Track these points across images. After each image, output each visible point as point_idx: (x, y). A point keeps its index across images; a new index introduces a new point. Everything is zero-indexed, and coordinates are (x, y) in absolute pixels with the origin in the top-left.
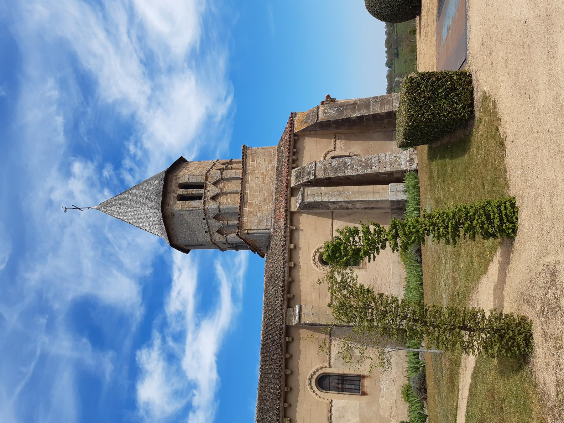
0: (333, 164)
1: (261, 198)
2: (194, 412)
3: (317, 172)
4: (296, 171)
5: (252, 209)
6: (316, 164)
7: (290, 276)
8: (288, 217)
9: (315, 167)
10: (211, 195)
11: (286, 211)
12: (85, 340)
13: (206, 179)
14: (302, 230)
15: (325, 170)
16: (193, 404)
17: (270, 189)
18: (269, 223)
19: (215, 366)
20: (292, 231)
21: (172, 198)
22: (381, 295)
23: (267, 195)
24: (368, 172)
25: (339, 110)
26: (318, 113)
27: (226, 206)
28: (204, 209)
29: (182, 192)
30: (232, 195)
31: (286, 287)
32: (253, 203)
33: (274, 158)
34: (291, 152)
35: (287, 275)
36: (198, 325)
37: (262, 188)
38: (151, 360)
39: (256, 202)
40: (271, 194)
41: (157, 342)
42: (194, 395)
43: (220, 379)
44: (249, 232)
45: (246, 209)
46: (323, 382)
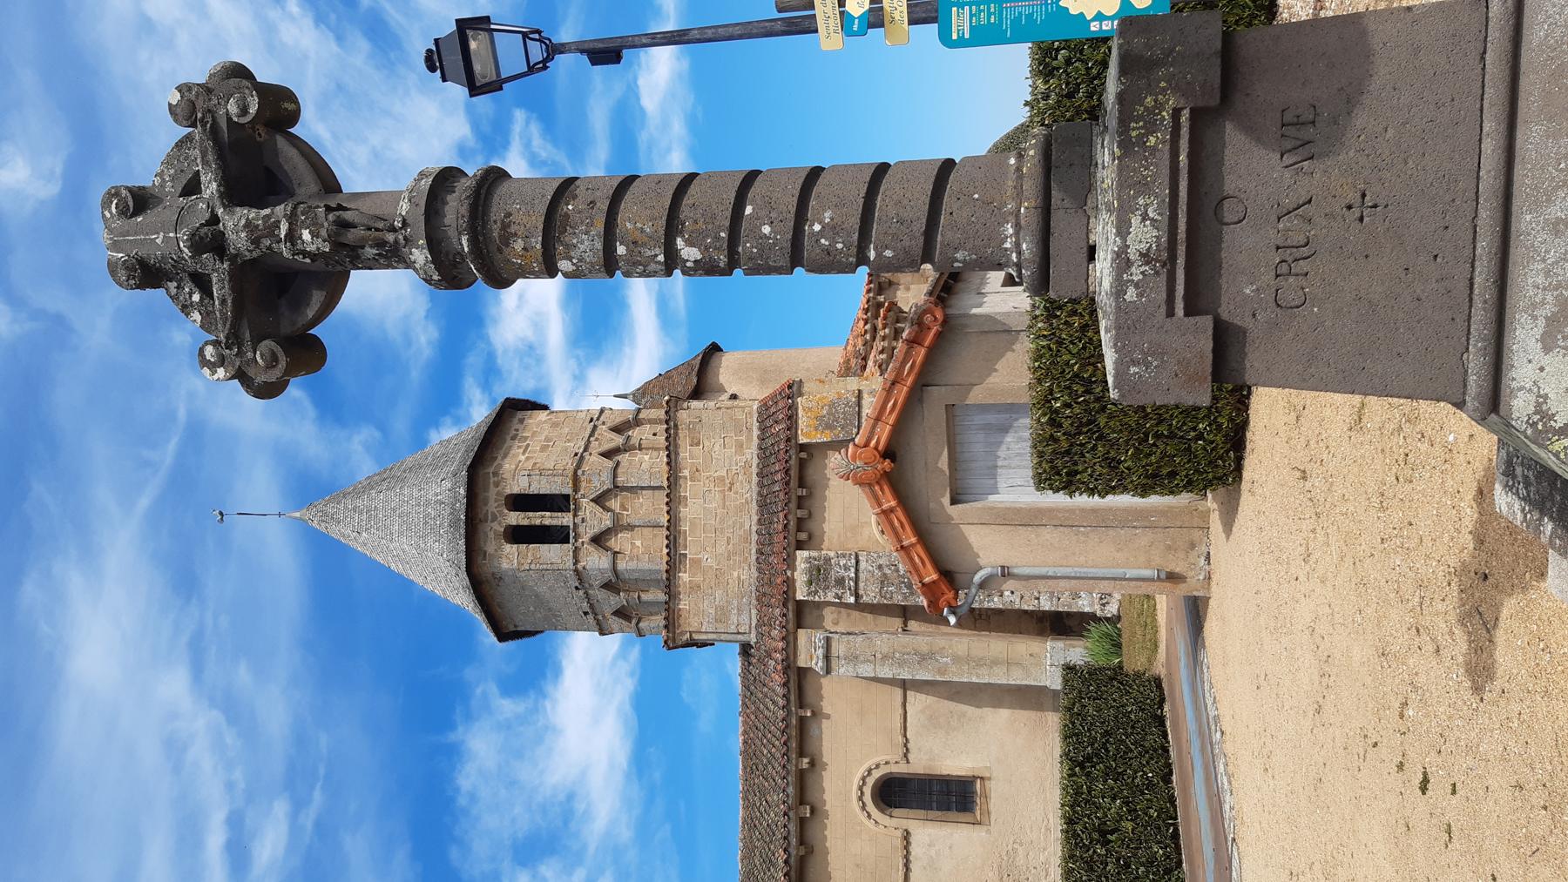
1: (721, 548)
3: (861, 585)
4: (808, 560)
5: (698, 579)
6: (857, 562)
7: (802, 841)
8: (792, 685)
9: (857, 570)
10: (591, 533)
11: (786, 670)
13: (576, 488)
14: (828, 717)
15: (884, 581)
17: (742, 525)
18: (745, 618)
20: (802, 721)
21: (491, 535)
23: (736, 540)
24: (992, 605)
27: (632, 565)
28: (576, 570)
29: (515, 518)
30: (646, 530)
31: (792, 473)
32: (700, 561)
33: (749, 439)
34: (794, 498)
35: (794, 841)
37: (722, 521)
39: (708, 560)
40: (747, 540)
44: (696, 637)
45: (684, 577)
46: (894, 793)
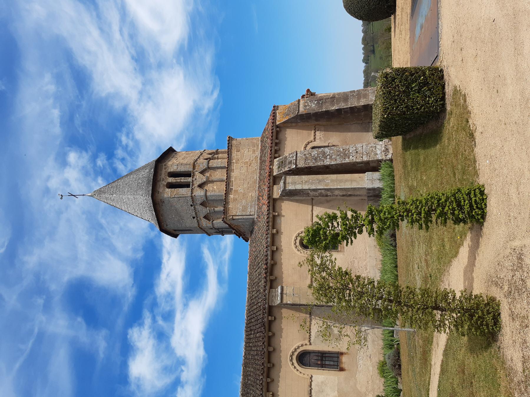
0: (313, 154)
1: (245, 186)
2: (182, 387)
3: (298, 161)
4: (278, 161)
5: (237, 196)
6: (297, 154)
7: (272, 259)
9: (296, 157)
10: (198, 183)
12: (79, 319)
13: (194, 168)
14: (284, 216)
15: (306, 159)
16: (182, 379)
17: (253, 178)
18: (253, 209)
19: (202, 344)
20: (274, 216)
21: (162, 186)
22: (358, 277)
23: (251, 183)
24: (345, 162)
25: (318, 103)
26: (299, 106)
27: (212, 194)
28: (192, 196)
29: (171, 180)
30: (218, 183)
31: (269, 269)
32: (237, 190)
33: (258, 148)
34: (274, 143)
35: (269, 258)
36: (186, 305)
37: (246, 176)
38: (142, 338)
39: (241, 190)
40: (255, 182)
41: (148, 321)
42: (182, 371)
43: (206, 356)
44: (234, 217)
45: (231, 196)
46: (304, 358)
